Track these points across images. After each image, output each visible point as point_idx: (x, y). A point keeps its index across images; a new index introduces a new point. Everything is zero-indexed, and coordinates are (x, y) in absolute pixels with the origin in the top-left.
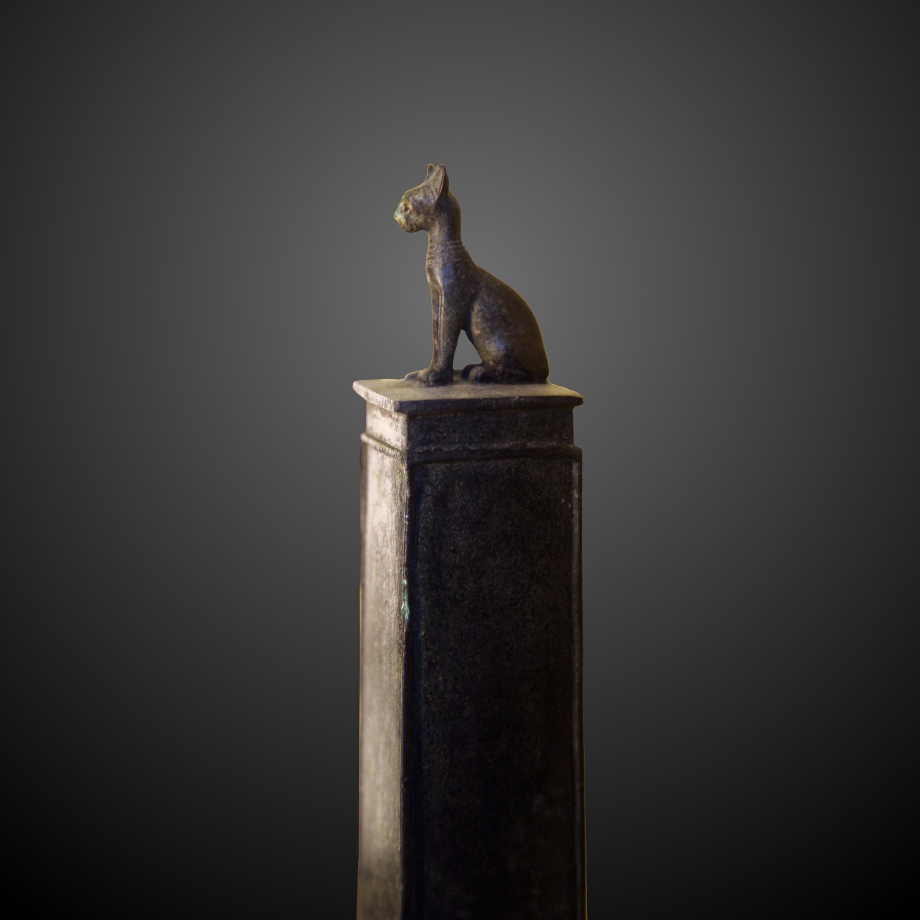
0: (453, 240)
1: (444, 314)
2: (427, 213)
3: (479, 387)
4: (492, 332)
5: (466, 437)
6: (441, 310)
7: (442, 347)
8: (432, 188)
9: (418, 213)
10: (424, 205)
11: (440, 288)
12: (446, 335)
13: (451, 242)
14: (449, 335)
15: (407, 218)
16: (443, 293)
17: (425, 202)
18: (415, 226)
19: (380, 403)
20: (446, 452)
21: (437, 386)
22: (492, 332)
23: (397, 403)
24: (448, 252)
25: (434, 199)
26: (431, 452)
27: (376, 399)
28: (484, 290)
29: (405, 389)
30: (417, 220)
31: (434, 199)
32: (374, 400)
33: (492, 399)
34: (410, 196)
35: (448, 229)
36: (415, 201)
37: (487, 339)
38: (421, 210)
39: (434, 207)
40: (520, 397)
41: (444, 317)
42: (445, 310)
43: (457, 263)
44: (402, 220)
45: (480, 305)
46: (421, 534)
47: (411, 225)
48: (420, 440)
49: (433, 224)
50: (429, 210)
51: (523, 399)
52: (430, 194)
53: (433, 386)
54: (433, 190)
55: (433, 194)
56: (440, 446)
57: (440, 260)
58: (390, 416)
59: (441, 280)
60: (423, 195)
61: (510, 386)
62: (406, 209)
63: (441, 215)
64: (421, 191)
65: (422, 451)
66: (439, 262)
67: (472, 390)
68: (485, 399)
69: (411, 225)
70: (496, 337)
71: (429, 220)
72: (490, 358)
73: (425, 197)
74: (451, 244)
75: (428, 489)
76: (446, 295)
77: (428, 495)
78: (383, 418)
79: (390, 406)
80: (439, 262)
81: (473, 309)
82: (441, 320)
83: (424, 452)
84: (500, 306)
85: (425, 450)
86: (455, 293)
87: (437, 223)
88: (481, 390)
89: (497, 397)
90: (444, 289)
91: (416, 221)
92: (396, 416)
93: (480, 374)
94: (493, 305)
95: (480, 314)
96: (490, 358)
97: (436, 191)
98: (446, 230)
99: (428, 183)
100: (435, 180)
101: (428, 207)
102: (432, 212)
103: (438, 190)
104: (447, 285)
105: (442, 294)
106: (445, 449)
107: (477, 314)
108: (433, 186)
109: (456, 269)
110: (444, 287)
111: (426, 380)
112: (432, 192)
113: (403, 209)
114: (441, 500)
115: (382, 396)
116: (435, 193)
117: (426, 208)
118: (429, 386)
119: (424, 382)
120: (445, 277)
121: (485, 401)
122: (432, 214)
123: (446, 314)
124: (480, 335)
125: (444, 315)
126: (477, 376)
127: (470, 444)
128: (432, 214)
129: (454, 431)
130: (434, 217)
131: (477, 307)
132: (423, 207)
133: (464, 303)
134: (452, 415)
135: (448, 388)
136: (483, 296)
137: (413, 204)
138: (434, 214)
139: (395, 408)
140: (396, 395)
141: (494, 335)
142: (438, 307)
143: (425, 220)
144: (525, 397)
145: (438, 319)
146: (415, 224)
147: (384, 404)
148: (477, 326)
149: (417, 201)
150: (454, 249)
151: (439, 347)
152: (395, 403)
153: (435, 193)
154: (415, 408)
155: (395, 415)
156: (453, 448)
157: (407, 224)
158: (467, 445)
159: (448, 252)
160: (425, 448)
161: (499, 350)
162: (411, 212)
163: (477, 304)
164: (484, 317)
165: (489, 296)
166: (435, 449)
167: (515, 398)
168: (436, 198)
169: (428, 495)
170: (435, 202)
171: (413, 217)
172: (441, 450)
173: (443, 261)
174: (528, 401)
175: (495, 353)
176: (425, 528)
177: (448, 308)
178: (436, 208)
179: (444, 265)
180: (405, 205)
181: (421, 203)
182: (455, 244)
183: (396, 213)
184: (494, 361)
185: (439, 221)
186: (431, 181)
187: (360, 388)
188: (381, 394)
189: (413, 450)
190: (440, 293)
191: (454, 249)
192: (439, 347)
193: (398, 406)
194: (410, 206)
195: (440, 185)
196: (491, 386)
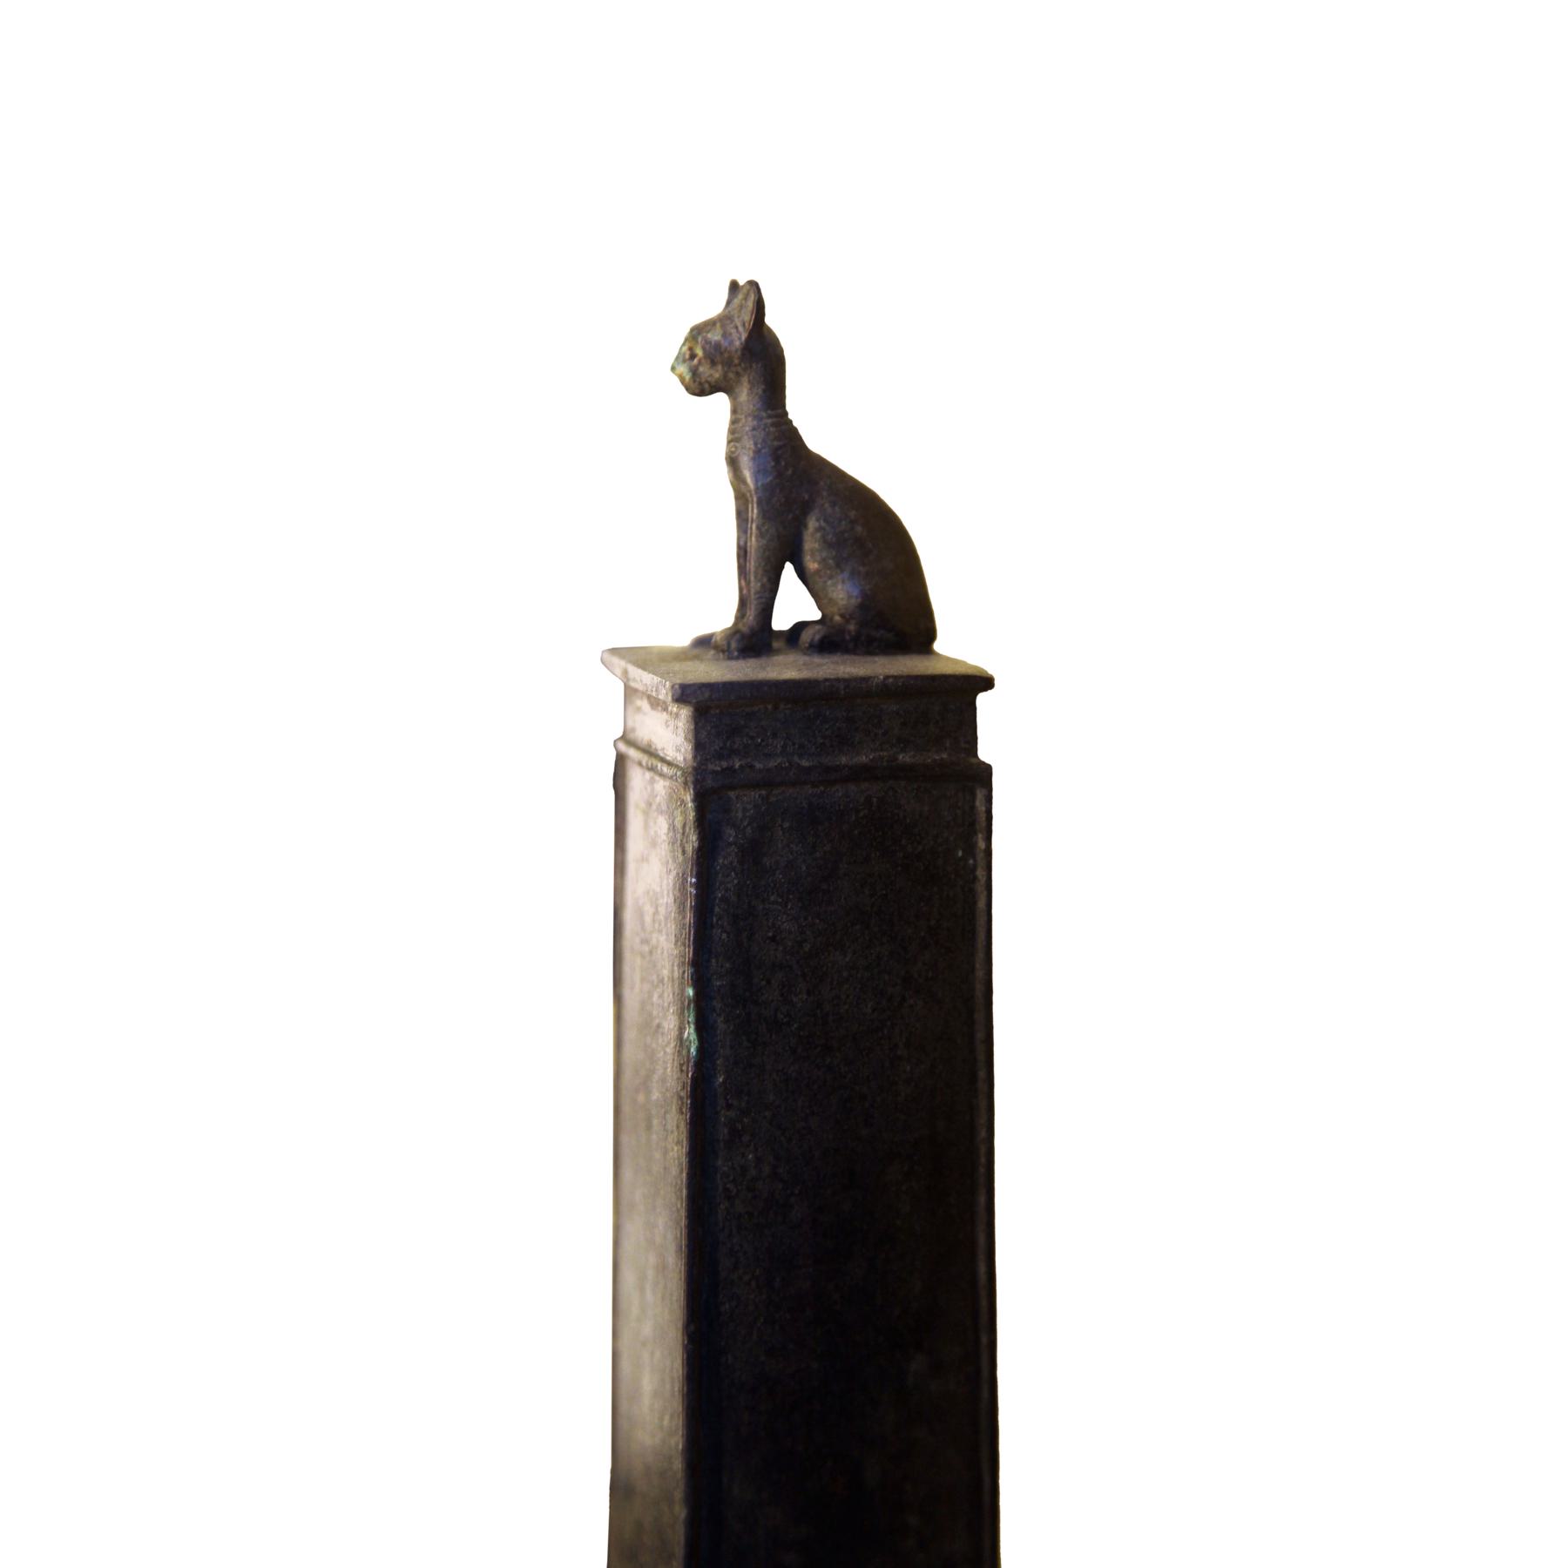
0: (772, 410)
1: (757, 535)
2: (728, 363)
3: (817, 659)
4: (838, 565)
5: (794, 744)
6: (751, 528)
8: (736, 320)
9: (713, 363)
10: (723, 349)
11: (750, 491)
12: (760, 571)
13: (769, 412)
14: (765, 571)
16: (755, 499)
17: (725, 344)
19: (647, 688)
20: (760, 771)
21: (744, 658)
22: (838, 565)
23: (677, 687)
24: (764, 429)
25: (740, 339)
26: (735, 771)
27: (641, 681)
28: (825, 494)
29: (690, 663)
30: (711, 375)
31: (740, 339)
32: (637, 681)
33: (838, 680)
35: (764, 391)
36: (707, 342)
37: (831, 577)
38: (718, 359)
39: (739, 353)
40: (887, 677)
41: (757, 541)
42: (758, 528)
43: (780, 447)
44: (684, 375)
45: (818, 520)
46: (717, 909)
47: (700, 384)
48: (715, 750)
49: (738, 382)
50: (730, 358)
51: (891, 680)
52: (733, 331)
53: (737, 658)
54: (739, 324)
55: (738, 331)
56: (749, 760)
57: (749, 444)
58: (665, 709)
59: (751, 478)
60: (721, 332)
61: (869, 658)
63: (751, 367)
65: (719, 769)
66: (748, 446)
67: (804, 664)
68: (826, 680)
69: (700, 384)
70: (846, 574)
71: (731, 375)
74: (769, 417)
75: (730, 834)
76: (759, 503)
77: (730, 844)
78: (654, 713)
79: (665, 692)
80: (748, 446)
81: (806, 526)
82: (751, 546)
83: (723, 770)
84: (852, 522)
85: (724, 767)
86: (775, 499)
87: (745, 380)
88: (819, 665)
89: (846, 676)
90: (756, 493)
91: (709, 376)
92: (675, 709)
93: (817, 637)
94: (840, 520)
95: (818, 535)
96: (835, 610)
97: (744, 325)
98: (760, 391)
101: (729, 352)
102: (736, 361)
103: (747, 324)
104: (763, 485)
105: (752, 501)
106: (758, 766)
107: (812, 535)
108: (739, 317)
109: (777, 459)
110: (757, 489)
111: (725, 648)
112: (737, 327)
113: (687, 356)
114: (752, 852)
115: (651, 675)
116: (741, 329)
117: (726, 355)
118: (730, 658)
119: (723, 651)
120: (759, 471)
121: (827, 683)
122: (736, 366)
123: (761, 535)
124: (818, 572)
125: (757, 537)
126: (812, 640)
127: (801, 756)
128: (736, 366)
129: (774, 735)
130: (739, 369)
131: (812, 523)
132: (721, 353)
133: (790, 516)
134: (770, 707)
135: (763, 660)
136: (823, 505)
137: (704, 348)
138: (740, 365)
139: (673, 696)
140: (675, 673)
141: (842, 571)
142: (747, 524)
143: (725, 376)
144: (895, 677)
146: (707, 382)
147: (654, 689)
148: (813, 555)
149: (710, 343)
150: (773, 425)
152: (673, 687)
153: (741, 329)
154: (707, 695)
155: (674, 708)
156: (772, 764)
157: (695, 381)
158: (796, 759)
159: (764, 429)
160: (725, 764)
161: (850, 597)
162: (700, 361)
163: (814, 518)
164: (824, 540)
165: (834, 504)
166: (741, 766)
167: (878, 679)
168: (743, 338)
169: (730, 844)
170: (741, 344)
171: (705, 370)
172: (752, 767)
173: (756, 444)
174: (900, 684)
175: (844, 602)
176: (724, 899)
177: (763, 524)
178: (743, 355)
179: (757, 452)
181: (717, 346)
182: (776, 416)
184: (842, 616)
185: (749, 377)
186: (734, 309)
188: (650, 672)
189: (703, 767)
190: (750, 499)
191: (773, 425)
193: (679, 691)
194: (699, 352)
195: (749, 315)
196: (836, 658)
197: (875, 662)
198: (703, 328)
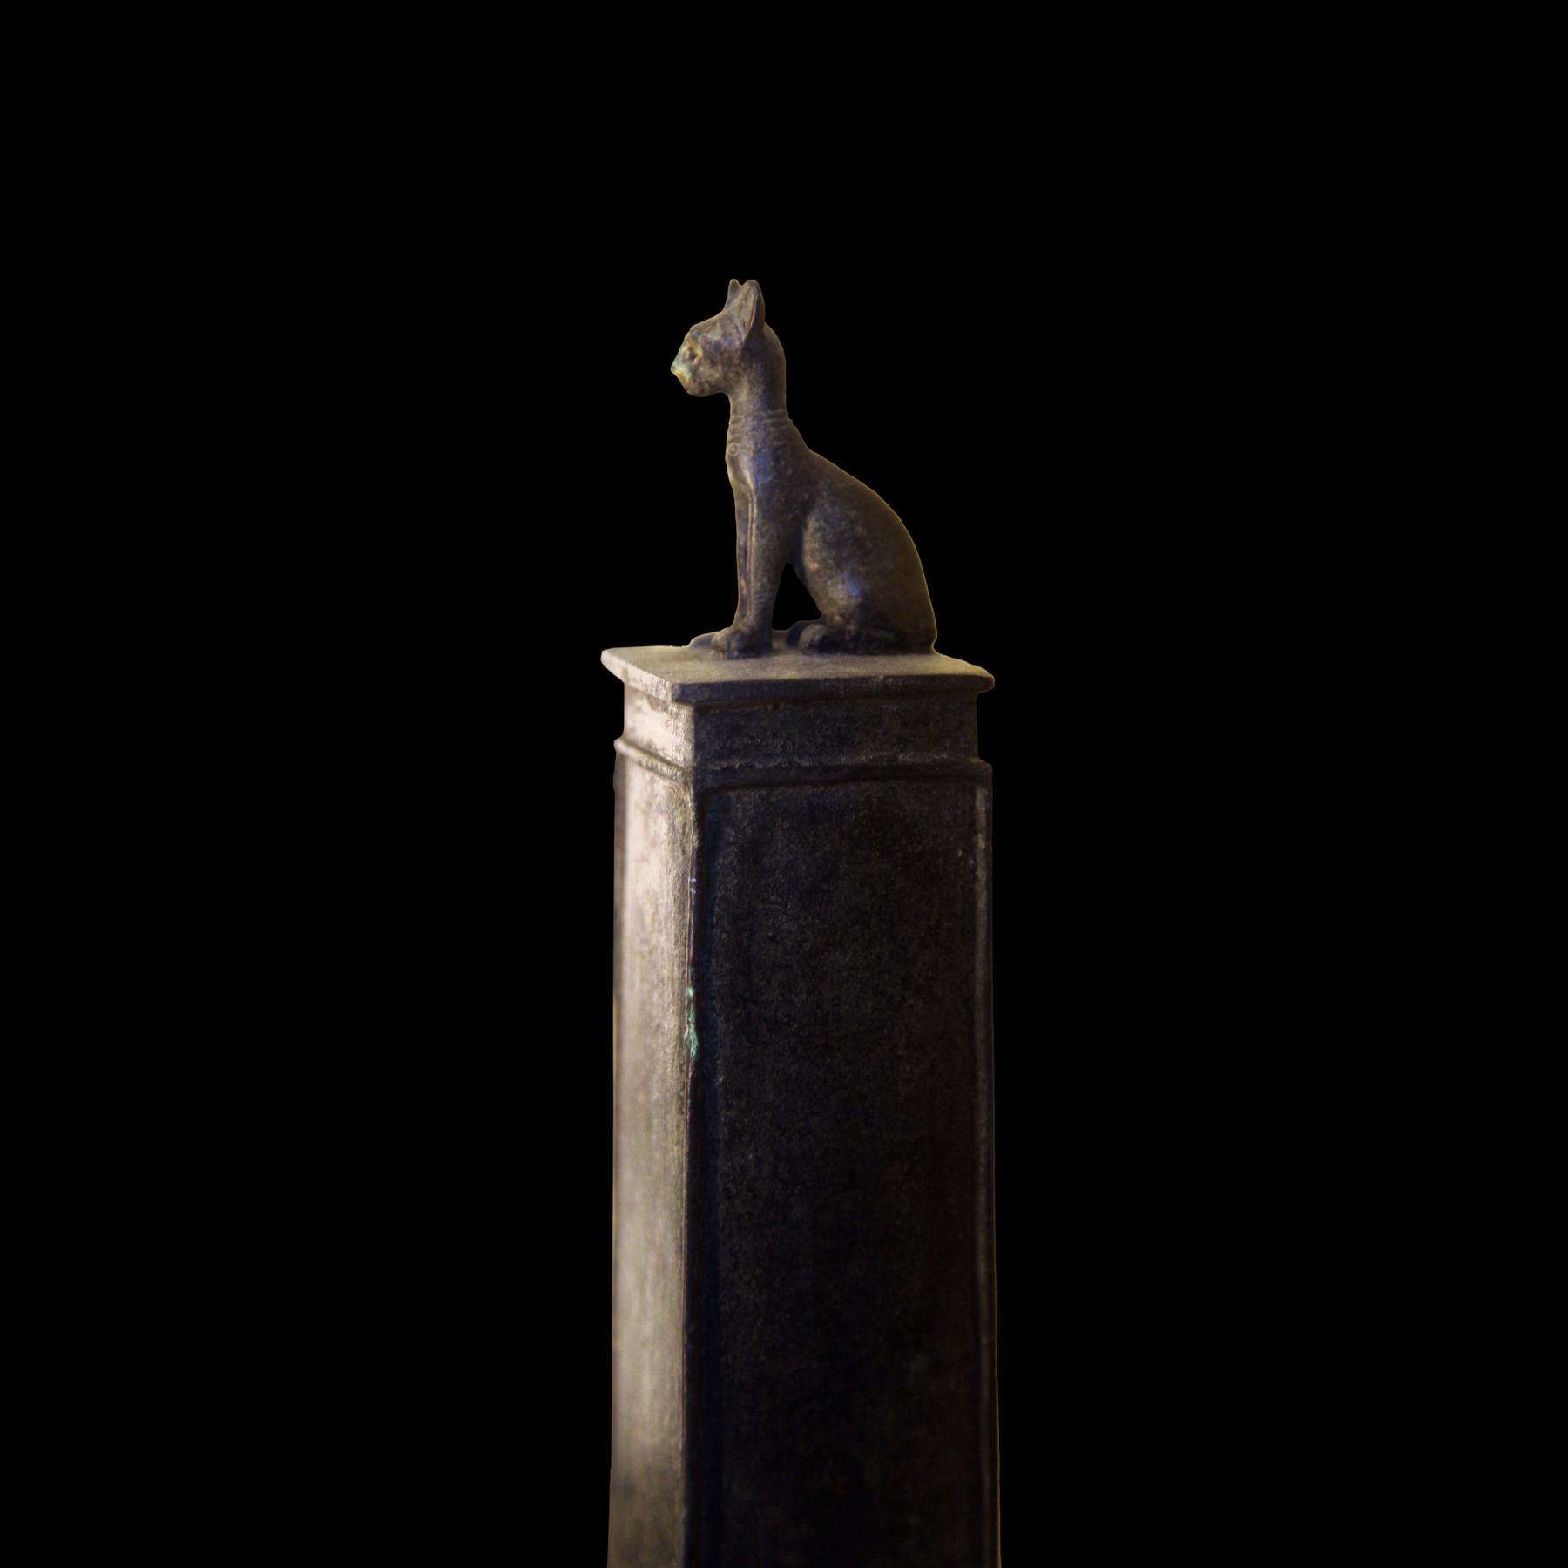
0: (772, 410)
1: (757, 535)
2: (728, 363)
3: (817, 659)
4: (838, 565)
5: (794, 744)
6: (751, 528)
7: (753, 591)
8: (736, 320)
9: (713, 363)
10: (723, 349)
11: (750, 491)
12: (760, 571)
13: (769, 412)
14: (765, 571)
15: (694, 372)
16: (755, 499)
17: (725, 344)
18: (707, 386)
19: (647, 688)
20: (760, 771)
21: (744, 658)
22: (838, 565)
23: (677, 687)
24: (764, 429)
25: (740, 339)
26: (735, 771)
27: (641, 681)
28: (825, 494)
29: (690, 663)
30: (711, 375)
31: (740, 339)
32: (637, 681)
33: (838, 680)
34: (699, 333)
35: (764, 391)
36: (707, 342)
37: (831, 577)
38: (718, 359)
39: (739, 353)
40: (887, 677)
41: (757, 541)
42: (758, 528)
43: (780, 447)
44: (684, 375)
45: (818, 520)
46: (717, 909)
47: (700, 384)
48: (715, 750)
49: (738, 382)
50: (730, 358)
51: (891, 680)
52: (733, 331)
53: (737, 658)
54: (739, 324)
55: (738, 331)
56: (749, 760)
57: (749, 444)
58: (665, 709)
59: (751, 478)
60: (721, 332)
61: (869, 658)
62: (693, 356)
63: (751, 367)
64: (718, 325)
65: (719, 769)
66: (748, 446)
67: (804, 664)
68: (826, 680)
69: (700, 384)
70: (846, 574)
71: (731, 375)
72: (835, 610)
73: (725, 335)
74: (769, 417)
75: (730, 834)
76: (759, 503)
77: (730, 844)
78: (654, 713)
80: (748, 446)
81: (806, 526)
82: (751, 546)
83: (723, 770)
84: (852, 522)
85: (724, 767)
86: (775, 499)
87: (745, 380)
88: (819, 665)
89: (846, 676)
90: (756, 493)
91: (709, 376)
92: (675, 709)
93: (817, 637)
94: (840, 520)
95: (818, 535)
96: (835, 610)
97: (744, 325)
98: (760, 391)
99: (729, 312)
100: (741, 307)
101: (729, 352)
102: (736, 361)
103: (747, 324)
104: (763, 485)
105: (752, 501)
106: (758, 766)
107: (812, 535)
108: (739, 317)
109: (777, 459)
110: (757, 489)
111: (725, 648)
112: (737, 327)
114: (752, 852)
115: (651, 675)
116: (741, 329)
117: (726, 355)
118: (730, 658)
119: (723, 651)
120: (759, 471)
121: (827, 683)
122: (736, 366)
123: (761, 535)
124: (818, 572)
125: (757, 537)
126: (812, 640)
127: (801, 756)
128: (736, 366)
129: (774, 735)
130: (739, 369)
131: (812, 523)
132: (721, 353)
133: (790, 516)
134: (770, 707)
135: (763, 660)
136: (823, 505)
137: (704, 348)
138: (740, 365)
139: (673, 696)
141: (842, 571)
142: (747, 524)
143: (725, 376)
144: (895, 677)
145: (746, 543)
146: (707, 382)
147: (654, 689)
148: (813, 555)
149: (710, 343)
150: (773, 425)
151: (749, 591)
152: (673, 687)
153: (741, 329)
154: (707, 695)
155: (674, 708)
156: (772, 764)
157: (695, 381)
158: (796, 759)
159: (764, 429)
160: (725, 764)
161: (850, 597)
162: (700, 361)
163: (814, 518)
164: (824, 540)
165: (834, 504)
166: (741, 766)
167: (878, 679)
168: (743, 338)
169: (730, 844)
170: (741, 344)
171: (705, 370)
172: (752, 767)
173: (756, 444)
174: (900, 684)
175: (844, 602)
176: (724, 899)
177: (763, 524)
178: (743, 355)
179: (757, 452)
180: (691, 349)
181: (717, 346)
183: (675, 364)
184: (842, 616)
185: (749, 377)
186: (734, 309)
187: (614, 661)
188: (650, 672)
189: (703, 767)
190: (750, 499)
191: (773, 425)
192: (749, 591)
193: (679, 691)
194: (699, 352)
195: (749, 315)
196: (836, 658)
197: (875, 662)
198: (703, 328)
